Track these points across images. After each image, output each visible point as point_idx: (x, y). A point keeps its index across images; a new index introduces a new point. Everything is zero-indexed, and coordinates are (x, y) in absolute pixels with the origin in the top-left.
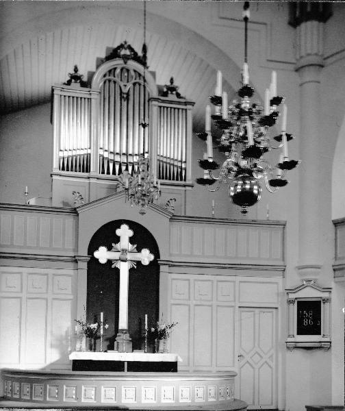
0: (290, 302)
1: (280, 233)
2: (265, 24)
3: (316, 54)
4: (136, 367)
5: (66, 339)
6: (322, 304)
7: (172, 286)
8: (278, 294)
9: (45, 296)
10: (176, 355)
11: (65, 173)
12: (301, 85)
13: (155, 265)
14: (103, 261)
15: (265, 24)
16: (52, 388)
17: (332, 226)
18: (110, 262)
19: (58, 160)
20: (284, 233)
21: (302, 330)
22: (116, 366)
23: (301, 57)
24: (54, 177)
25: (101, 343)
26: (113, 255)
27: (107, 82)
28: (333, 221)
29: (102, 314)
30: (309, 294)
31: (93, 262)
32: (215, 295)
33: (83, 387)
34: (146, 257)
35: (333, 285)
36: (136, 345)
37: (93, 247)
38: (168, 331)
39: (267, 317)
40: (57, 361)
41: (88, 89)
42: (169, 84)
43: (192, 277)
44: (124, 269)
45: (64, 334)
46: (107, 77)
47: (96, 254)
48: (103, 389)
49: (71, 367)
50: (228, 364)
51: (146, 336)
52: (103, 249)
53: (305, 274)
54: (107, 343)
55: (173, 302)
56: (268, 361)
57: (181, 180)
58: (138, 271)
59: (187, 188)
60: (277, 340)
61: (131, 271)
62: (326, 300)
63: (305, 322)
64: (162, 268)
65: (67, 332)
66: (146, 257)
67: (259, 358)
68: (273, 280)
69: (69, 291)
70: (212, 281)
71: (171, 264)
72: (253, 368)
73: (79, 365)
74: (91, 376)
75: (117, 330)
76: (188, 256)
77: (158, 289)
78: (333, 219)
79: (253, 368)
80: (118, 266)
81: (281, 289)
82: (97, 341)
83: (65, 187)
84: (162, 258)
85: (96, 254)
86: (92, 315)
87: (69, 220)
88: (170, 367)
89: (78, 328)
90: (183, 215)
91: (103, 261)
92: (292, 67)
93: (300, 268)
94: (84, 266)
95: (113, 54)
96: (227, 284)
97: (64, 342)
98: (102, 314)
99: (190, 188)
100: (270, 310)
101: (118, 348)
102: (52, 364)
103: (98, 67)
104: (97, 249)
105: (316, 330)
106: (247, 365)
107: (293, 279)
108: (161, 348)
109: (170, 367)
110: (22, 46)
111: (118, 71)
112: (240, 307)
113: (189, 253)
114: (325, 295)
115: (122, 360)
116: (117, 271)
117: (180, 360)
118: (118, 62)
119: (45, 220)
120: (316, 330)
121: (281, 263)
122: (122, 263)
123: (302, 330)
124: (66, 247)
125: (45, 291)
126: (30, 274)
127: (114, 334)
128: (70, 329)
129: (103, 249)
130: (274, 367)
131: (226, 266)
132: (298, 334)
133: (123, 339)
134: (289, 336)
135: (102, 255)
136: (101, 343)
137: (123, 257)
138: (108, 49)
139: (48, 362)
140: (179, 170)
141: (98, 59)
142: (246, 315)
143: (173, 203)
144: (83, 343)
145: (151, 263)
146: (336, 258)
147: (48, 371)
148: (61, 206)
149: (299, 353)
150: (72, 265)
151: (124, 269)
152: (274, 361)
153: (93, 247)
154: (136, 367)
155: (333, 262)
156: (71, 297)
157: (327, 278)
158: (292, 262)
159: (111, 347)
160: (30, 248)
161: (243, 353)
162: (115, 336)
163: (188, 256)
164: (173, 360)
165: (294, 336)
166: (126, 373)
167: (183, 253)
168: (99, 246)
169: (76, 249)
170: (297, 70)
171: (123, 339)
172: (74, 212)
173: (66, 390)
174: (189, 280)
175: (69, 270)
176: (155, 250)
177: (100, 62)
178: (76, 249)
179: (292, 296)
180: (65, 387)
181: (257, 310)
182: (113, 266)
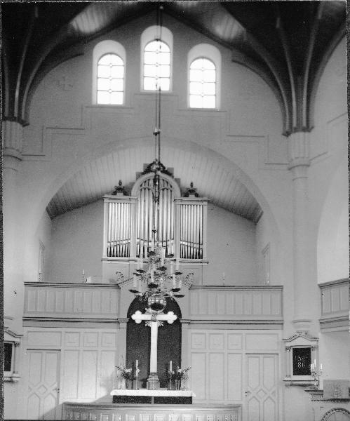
0: (287, 349)
1: (279, 296)
2: (263, 137)
3: (18, 150)
4: (160, 400)
5: (111, 380)
6: (13, 347)
7: (191, 338)
8: (278, 342)
9: (78, 348)
10: (192, 391)
11: (112, 258)
12: (293, 180)
13: (178, 323)
14: (138, 322)
15: (263, 137)
17: (318, 289)
18: (143, 322)
22: (145, 400)
24: (104, 262)
25: (137, 382)
26: (146, 317)
27: (143, 190)
28: (319, 285)
30: (302, 343)
31: (131, 322)
35: (320, 335)
36: (163, 384)
38: (184, 373)
39: (269, 361)
41: (129, 197)
43: (63, 330)
44: (154, 328)
45: (109, 375)
47: (134, 317)
50: (235, 399)
51: (171, 378)
52: (138, 313)
53: (299, 327)
55: (192, 351)
56: (271, 396)
58: (164, 326)
59: (203, 264)
60: (278, 378)
61: (159, 328)
62: (16, 345)
64: (184, 326)
65: (112, 375)
66: (171, 317)
67: (264, 394)
72: (259, 401)
73: (117, 399)
74: (118, 407)
75: (149, 373)
76: (249, 316)
77: (150, 343)
78: (319, 283)
79: (259, 401)
83: (111, 269)
84: (184, 317)
85: (134, 317)
86: (130, 361)
87: (114, 292)
88: (187, 401)
89: (119, 373)
91: (138, 322)
92: (285, 167)
93: (295, 322)
94: (124, 325)
95: (148, 169)
96: (235, 337)
97: (110, 382)
99: (206, 264)
100: (273, 355)
102: (100, 399)
103: (137, 179)
104: (134, 313)
106: (269, 399)
107: (289, 331)
108: (182, 386)
109: (187, 401)
111: (151, 182)
113: (52, 311)
114: (313, 344)
115: (150, 395)
117: (194, 396)
118: (151, 175)
119: (97, 292)
120: (306, 371)
121: (280, 318)
122: (153, 323)
124: (38, 310)
130: (276, 401)
133: (153, 380)
135: (138, 317)
137: (154, 318)
138: (145, 165)
139: (98, 397)
142: (254, 361)
143: (191, 277)
144: (123, 383)
146: (322, 314)
148: (108, 282)
149: (294, 389)
151: (154, 328)
152: (277, 396)
153: (131, 311)
154: (160, 400)
155: (22, 315)
156: (115, 349)
157: (315, 329)
158: (288, 319)
159: (144, 386)
160: (87, 314)
161: (249, 390)
162: (148, 378)
163: (249, 316)
164: (189, 396)
165: (290, 376)
166: (153, 404)
167: (209, 313)
168: (137, 310)
170: (290, 169)
171: (153, 380)
172: (117, 286)
175: (112, 329)
176: (178, 312)
177: (139, 175)
179: (288, 344)
181: (44, 352)
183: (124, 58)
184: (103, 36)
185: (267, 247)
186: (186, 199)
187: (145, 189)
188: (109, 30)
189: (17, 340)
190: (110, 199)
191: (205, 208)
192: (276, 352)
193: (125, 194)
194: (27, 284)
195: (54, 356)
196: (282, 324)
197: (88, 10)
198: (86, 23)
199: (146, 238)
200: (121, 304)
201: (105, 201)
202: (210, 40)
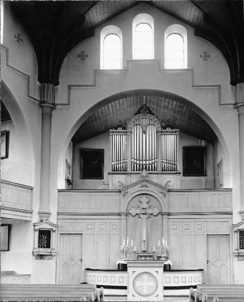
112: (61, 234)
183: (153, 26)
184: (106, 24)
185: (221, 163)
186: (163, 130)
187: (137, 125)
188: (109, 20)
189: (54, 229)
190: (113, 132)
191: (178, 136)
192: (228, 234)
193: (124, 128)
194: (59, 191)
195: (78, 238)
196: (232, 214)
197: (97, 6)
198: (95, 15)
199: (135, 158)
200: (216, 223)
201: (110, 134)
202: (181, 22)
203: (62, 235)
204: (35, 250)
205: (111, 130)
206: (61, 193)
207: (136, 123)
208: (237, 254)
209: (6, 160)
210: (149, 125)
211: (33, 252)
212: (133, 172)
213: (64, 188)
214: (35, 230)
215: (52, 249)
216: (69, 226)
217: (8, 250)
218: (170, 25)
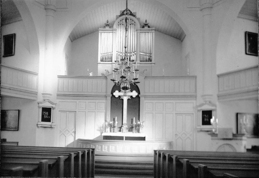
0: (198, 111)
4: (128, 138)
7: (145, 104)
9: (95, 111)
11: (103, 62)
16: (93, 146)
17: (216, 78)
18: (119, 97)
19: (139, 55)
20: (196, 81)
21: (44, 120)
22: (121, 138)
23: (203, 5)
25: (116, 129)
26: (121, 94)
29: (116, 117)
32: (154, 109)
33: (103, 146)
34: (134, 94)
36: (131, 129)
37: (113, 91)
40: (99, 136)
42: (145, 22)
44: (125, 99)
45: (102, 126)
46: (120, 23)
47: (114, 94)
48: (110, 146)
49: (103, 138)
52: (117, 92)
54: (119, 129)
57: (150, 61)
61: (128, 100)
63: (205, 120)
68: (192, 101)
69: (104, 108)
70: (163, 103)
71: (145, 97)
73: (107, 138)
80: (123, 98)
81: (195, 106)
82: (115, 128)
85: (114, 94)
88: (143, 139)
89: (107, 123)
90: (151, 76)
94: (109, 99)
95: (122, 14)
97: (102, 129)
98: (116, 117)
99: (154, 65)
101: (122, 131)
103: (116, 19)
105: (49, 120)
107: (200, 101)
109: (143, 139)
110: (53, 17)
112: (59, 111)
116: (123, 100)
118: (124, 17)
120: (49, 120)
123: (44, 120)
125: (95, 109)
126: (89, 102)
127: (121, 125)
128: (104, 124)
129: (117, 92)
131: (169, 96)
132: (42, 121)
134: (198, 126)
136: (116, 129)
140: (149, 57)
141: (117, 16)
143: (145, 72)
145: (137, 96)
146: (219, 91)
147: (96, 140)
148: (101, 75)
150: (105, 98)
151: (125, 99)
153: (113, 91)
154: (128, 138)
158: (199, 93)
168: (116, 90)
169: (106, 92)
170: (201, 10)
171: (125, 127)
173: (98, 147)
174: (153, 103)
176: (138, 91)
177: (117, 17)
178: (106, 92)
179: (199, 108)
180: (97, 146)
182: (121, 98)
186: (142, 29)
189: (54, 106)
191: (154, 34)
201: (99, 31)
203: (60, 112)
204: (39, 123)
205: (100, 29)
206: (221, 79)
207: (120, 23)
208: (199, 130)
209: (17, 132)
210: (131, 24)
211: (37, 125)
212: (101, 62)
213: (64, 75)
214: (39, 107)
215: (52, 123)
216: (70, 104)
217: (18, 130)
218: (39, 57)
